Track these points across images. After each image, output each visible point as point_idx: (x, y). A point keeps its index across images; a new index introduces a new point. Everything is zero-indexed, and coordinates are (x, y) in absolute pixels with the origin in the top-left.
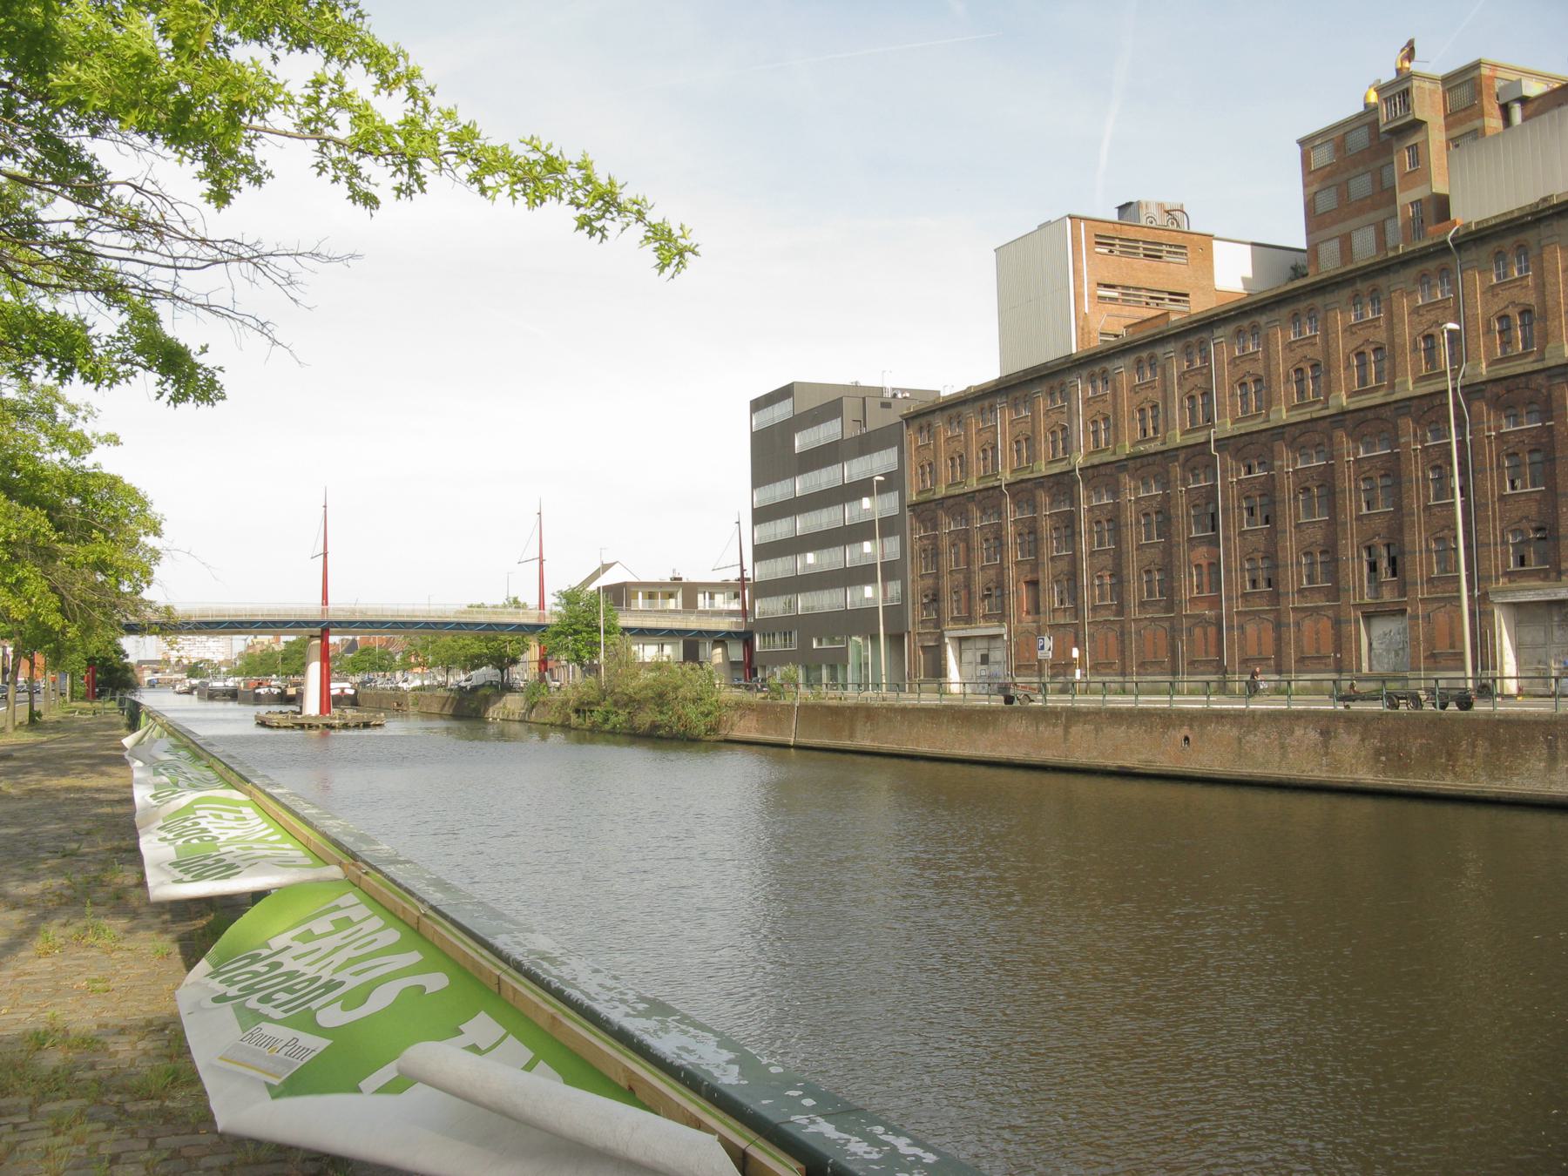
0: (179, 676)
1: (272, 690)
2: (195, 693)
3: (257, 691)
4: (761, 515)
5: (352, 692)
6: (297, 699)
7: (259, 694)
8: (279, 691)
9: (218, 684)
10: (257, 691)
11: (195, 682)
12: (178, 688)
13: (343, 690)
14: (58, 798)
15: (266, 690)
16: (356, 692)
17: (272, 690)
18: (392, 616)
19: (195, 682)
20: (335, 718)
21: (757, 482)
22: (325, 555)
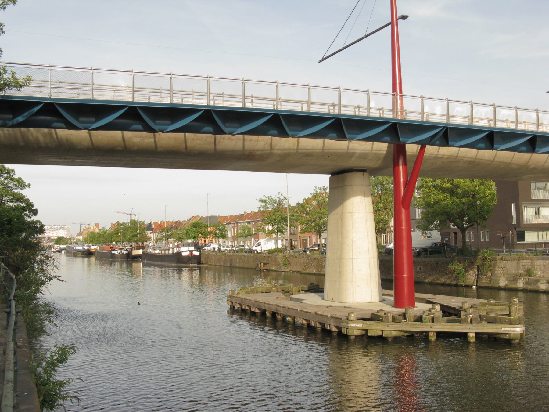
2: (63, 252)
3: (113, 252)
7: (114, 254)
9: (79, 248)
10: (113, 252)
11: (62, 246)
13: (191, 252)
15: (119, 251)
16: (200, 254)
17: (123, 251)
19: (62, 246)
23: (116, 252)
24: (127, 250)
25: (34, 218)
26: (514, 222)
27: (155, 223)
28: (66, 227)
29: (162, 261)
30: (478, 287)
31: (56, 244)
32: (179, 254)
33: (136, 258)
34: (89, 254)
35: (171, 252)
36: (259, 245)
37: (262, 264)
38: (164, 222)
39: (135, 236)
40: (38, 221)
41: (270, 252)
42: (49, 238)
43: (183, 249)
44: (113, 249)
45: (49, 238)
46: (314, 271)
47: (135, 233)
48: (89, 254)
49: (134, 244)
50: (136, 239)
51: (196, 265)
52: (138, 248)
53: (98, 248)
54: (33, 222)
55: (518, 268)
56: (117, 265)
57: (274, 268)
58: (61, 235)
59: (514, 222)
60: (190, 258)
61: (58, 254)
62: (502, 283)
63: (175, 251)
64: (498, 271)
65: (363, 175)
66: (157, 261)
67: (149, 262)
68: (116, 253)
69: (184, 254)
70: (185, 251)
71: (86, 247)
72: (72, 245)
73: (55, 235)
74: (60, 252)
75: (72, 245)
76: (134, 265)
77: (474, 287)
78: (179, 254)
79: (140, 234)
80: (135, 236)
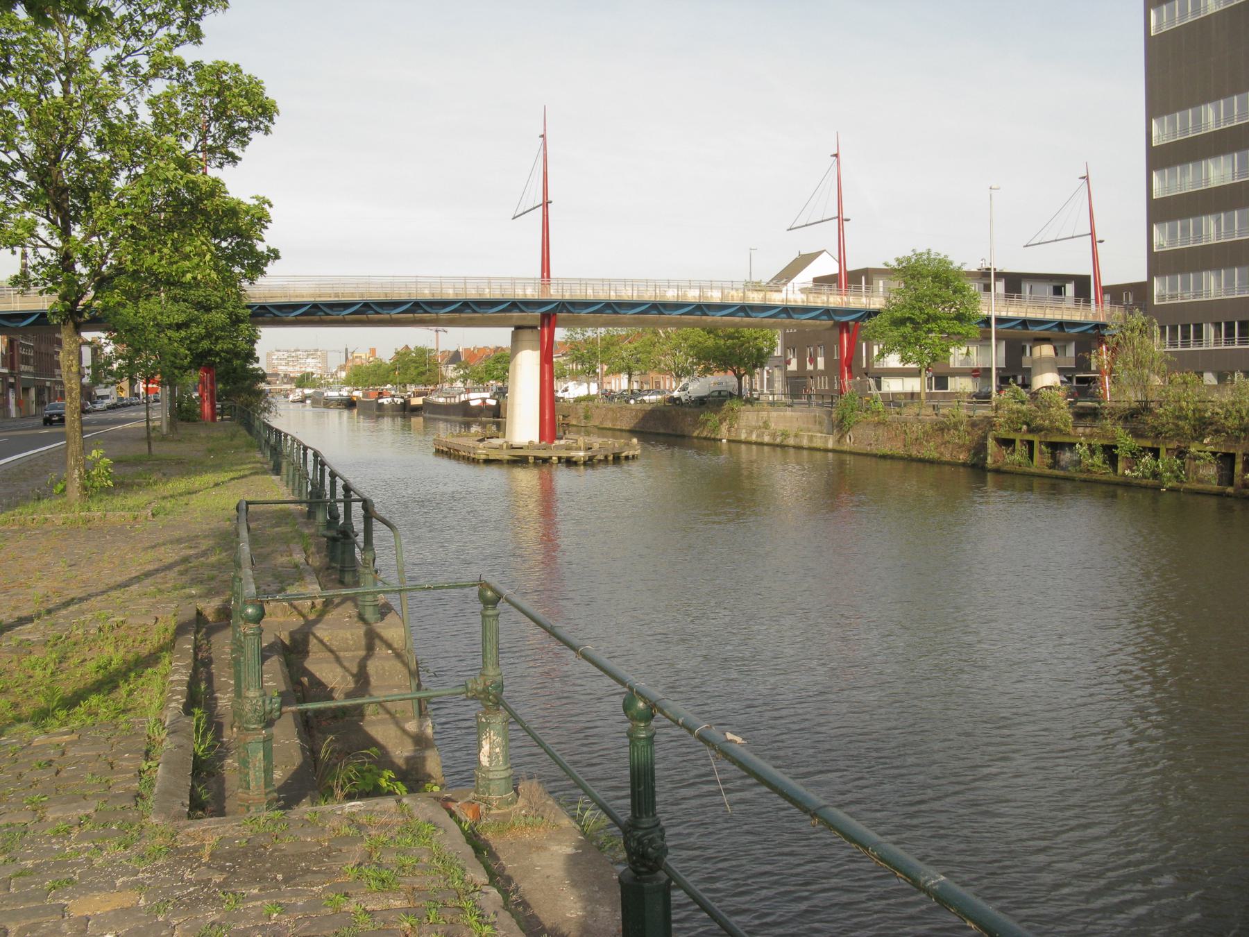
0: (288, 387)
1: (396, 399)
2: (308, 402)
3: (380, 401)
4: (1159, 158)
5: (493, 402)
6: (496, 415)
7: (382, 404)
8: (402, 400)
9: (333, 394)
10: (380, 401)
11: (308, 391)
12: (291, 397)
13: (484, 400)
14: (26, 538)
15: (390, 399)
16: (498, 402)
17: (396, 399)
18: (311, 296)
19: (308, 391)
20: (579, 449)
21: (1156, 106)
22: (546, 204)
23: (386, 401)
24: (402, 398)
25: (256, 366)
26: (864, 366)
27: (467, 350)
28: (319, 353)
29: (447, 414)
30: (729, 441)
31: (299, 386)
32: (467, 402)
33: (416, 410)
34: (350, 404)
35: (457, 401)
36: (566, 390)
37: (561, 417)
38: (479, 349)
39: (423, 373)
40: (260, 369)
41: (578, 400)
42: (286, 376)
43: (472, 395)
44: (381, 395)
45: (286, 376)
46: (610, 426)
47: (422, 369)
48: (350, 404)
49: (412, 388)
50: (424, 378)
51: (491, 419)
52: (419, 394)
53: (361, 395)
54: (257, 370)
55: (758, 420)
56: (386, 423)
57: (574, 422)
58: (309, 370)
59: (864, 366)
60: (483, 409)
61: (300, 405)
62: (743, 437)
63: (463, 398)
64: (743, 422)
65: (373, 351)
66: (440, 414)
67: (432, 416)
68: (386, 403)
69: (473, 403)
70: (475, 399)
71: (345, 393)
72: (322, 390)
73: (297, 368)
74: (303, 401)
75: (322, 390)
76: (413, 420)
77: (724, 441)
78: (467, 402)
79: (429, 370)
80: (423, 373)
